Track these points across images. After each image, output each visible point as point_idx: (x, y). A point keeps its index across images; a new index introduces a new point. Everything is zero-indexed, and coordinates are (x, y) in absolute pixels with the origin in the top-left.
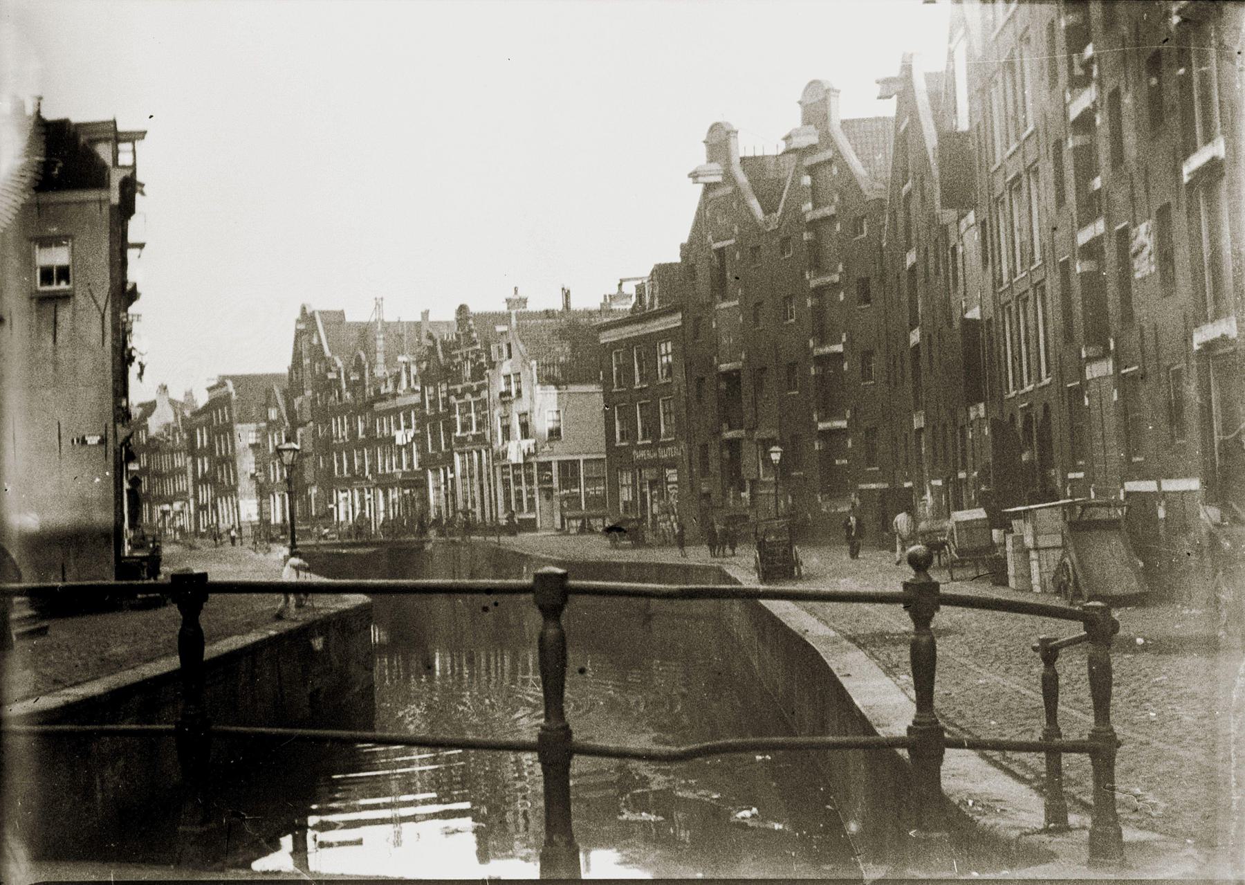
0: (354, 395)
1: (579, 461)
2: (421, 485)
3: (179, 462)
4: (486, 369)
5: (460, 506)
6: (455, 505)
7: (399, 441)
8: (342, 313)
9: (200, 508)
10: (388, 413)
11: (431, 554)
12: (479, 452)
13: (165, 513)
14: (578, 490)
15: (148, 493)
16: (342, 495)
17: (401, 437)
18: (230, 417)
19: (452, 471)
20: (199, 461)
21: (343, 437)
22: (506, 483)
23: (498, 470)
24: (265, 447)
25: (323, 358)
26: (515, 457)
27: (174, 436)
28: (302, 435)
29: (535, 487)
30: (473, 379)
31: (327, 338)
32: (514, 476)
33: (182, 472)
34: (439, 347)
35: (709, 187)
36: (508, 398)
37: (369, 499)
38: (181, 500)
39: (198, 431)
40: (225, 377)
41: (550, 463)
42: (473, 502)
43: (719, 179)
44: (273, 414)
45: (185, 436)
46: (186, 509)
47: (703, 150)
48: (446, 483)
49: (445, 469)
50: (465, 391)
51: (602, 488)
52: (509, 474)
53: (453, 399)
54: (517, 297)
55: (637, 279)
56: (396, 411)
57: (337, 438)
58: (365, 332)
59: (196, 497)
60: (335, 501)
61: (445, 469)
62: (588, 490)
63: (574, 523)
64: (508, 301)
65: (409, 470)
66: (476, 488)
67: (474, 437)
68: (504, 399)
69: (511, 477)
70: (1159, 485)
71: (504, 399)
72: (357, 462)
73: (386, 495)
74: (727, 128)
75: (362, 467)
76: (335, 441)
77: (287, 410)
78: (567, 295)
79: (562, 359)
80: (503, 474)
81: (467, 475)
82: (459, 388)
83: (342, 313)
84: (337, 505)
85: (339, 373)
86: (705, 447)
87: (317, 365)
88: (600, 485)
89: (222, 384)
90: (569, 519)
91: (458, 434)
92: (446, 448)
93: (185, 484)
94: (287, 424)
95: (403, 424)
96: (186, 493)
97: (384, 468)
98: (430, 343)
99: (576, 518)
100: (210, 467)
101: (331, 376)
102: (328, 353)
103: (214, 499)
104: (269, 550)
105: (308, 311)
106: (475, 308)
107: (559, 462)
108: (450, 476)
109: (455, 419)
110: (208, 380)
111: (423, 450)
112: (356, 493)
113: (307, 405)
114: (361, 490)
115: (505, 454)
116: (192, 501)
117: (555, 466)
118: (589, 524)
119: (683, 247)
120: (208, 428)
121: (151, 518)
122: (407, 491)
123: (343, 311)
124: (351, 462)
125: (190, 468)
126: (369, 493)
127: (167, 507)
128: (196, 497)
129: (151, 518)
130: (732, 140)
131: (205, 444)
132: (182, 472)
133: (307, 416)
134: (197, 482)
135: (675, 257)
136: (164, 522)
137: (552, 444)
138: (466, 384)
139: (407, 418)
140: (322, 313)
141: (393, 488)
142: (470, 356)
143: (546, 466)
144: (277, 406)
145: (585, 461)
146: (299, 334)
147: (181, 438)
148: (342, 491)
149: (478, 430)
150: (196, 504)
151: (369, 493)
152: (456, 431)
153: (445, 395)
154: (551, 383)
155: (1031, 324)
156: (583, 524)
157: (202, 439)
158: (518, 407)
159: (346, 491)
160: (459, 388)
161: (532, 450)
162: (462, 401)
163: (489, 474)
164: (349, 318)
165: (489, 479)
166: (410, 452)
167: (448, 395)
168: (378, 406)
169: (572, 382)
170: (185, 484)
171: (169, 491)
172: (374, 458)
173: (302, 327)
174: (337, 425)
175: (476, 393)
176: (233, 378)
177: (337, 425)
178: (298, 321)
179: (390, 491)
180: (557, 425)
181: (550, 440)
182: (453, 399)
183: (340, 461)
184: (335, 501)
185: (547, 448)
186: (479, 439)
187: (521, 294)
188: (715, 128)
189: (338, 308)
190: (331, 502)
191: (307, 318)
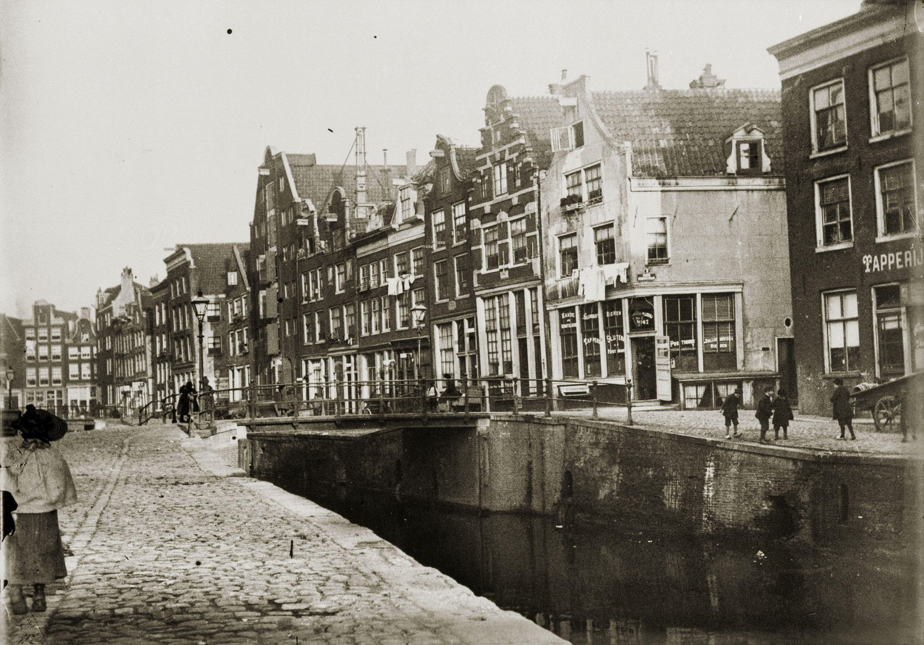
0: (330, 244)
1: (694, 296)
3: (139, 342)
4: (534, 170)
5: (485, 371)
6: (474, 372)
7: (392, 291)
8: (313, 157)
9: (159, 387)
10: (373, 258)
11: (486, 438)
12: (520, 294)
13: (126, 394)
14: (692, 342)
15: (112, 376)
16: (312, 367)
17: (394, 286)
19: (473, 322)
20: (158, 339)
21: (316, 296)
22: (568, 337)
23: (554, 317)
24: (225, 320)
25: (293, 205)
26: (593, 292)
27: (134, 315)
28: (264, 297)
29: (626, 339)
30: (511, 189)
31: (296, 182)
32: (582, 321)
33: (142, 351)
34: (453, 157)
36: (576, 206)
37: (349, 369)
38: (140, 380)
39: (157, 308)
41: (651, 298)
42: (508, 366)
44: (232, 279)
45: (144, 314)
46: (144, 390)
48: (461, 342)
49: (460, 323)
50: (496, 209)
51: (730, 338)
52: (574, 320)
56: (387, 254)
57: (308, 298)
58: (339, 176)
59: (154, 377)
60: (304, 374)
61: (460, 323)
62: (708, 341)
63: (691, 391)
66: (515, 345)
67: (511, 271)
68: (568, 208)
69: (577, 325)
70: (595, 413)
71: (568, 208)
72: (333, 325)
73: (371, 363)
75: (340, 330)
76: (305, 302)
77: (248, 273)
78: (652, 58)
79: (663, 144)
80: (562, 321)
81: (497, 329)
82: (487, 207)
83: (313, 157)
84: (307, 378)
85: (310, 219)
87: (283, 215)
88: (726, 335)
89: (180, 251)
90: (686, 384)
91: (484, 271)
92: (463, 291)
93: (144, 364)
94: (248, 289)
95: (397, 269)
96: (145, 373)
97: (369, 329)
99: (696, 384)
100: (168, 345)
101: (300, 222)
103: (171, 378)
104: (214, 432)
105: (274, 153)
107: (664, 297)
108: (468, 330)
109: (480, 250)
110: (166, 249)
111: (428, 300)
112: (332, 363)
113: (271, 266)
114: (338, 358)
115: (572, 291)
116: (150, 381)
117: (658, 305)
118: (717, 393)
120: (166, 303)
121: (114, 401)
122: (404, 355)
123: (314, 155)
124: (325, 325)
125: (149, 347)
126: (349, 361)
127: (127, 388)
128: (154, 377)
129: (114, 401)
131: (164, 320)
132: (142, 351)
133: (270, 276)
134: (156, 361)
136: (125, 402)
137: (654, 269)
139: (404, 264)
140: (288, 156)
141: (382, 353)
142: (507, 157)
143: (642, 305)
144: (237, 269)
145: (703, 295)
147: (140, 316)
148: (313, 361)
149: (517, 261)
150: (154, 384)
151: (349, 361)
152: (480, 268)
153: (462, 221)
154: (651, 175)
156: (708, 392)
157: (160, 317)
158: (593, 216)
159: (318, 361)
160: (487, 207)
161: (624, 279)
163: (535, 325)
164: (320, 161)
165: (535, 330)
166: (407, 305)
168: (361, 251)
169: (685, 175)
170: (144, 364)
171: (129, 373)
172: (357, 315)
173: (266, 172)
174: (307, 283)
176: (189, 247)
177: (307, 283)
179: (378, 357)
180: (661, 240)
181: (651, 264)
183: (311, 326)
184: (304, 374)
185: (647, 276)
189: (308, 152)
190: (299, 375)
191: (272, 161)
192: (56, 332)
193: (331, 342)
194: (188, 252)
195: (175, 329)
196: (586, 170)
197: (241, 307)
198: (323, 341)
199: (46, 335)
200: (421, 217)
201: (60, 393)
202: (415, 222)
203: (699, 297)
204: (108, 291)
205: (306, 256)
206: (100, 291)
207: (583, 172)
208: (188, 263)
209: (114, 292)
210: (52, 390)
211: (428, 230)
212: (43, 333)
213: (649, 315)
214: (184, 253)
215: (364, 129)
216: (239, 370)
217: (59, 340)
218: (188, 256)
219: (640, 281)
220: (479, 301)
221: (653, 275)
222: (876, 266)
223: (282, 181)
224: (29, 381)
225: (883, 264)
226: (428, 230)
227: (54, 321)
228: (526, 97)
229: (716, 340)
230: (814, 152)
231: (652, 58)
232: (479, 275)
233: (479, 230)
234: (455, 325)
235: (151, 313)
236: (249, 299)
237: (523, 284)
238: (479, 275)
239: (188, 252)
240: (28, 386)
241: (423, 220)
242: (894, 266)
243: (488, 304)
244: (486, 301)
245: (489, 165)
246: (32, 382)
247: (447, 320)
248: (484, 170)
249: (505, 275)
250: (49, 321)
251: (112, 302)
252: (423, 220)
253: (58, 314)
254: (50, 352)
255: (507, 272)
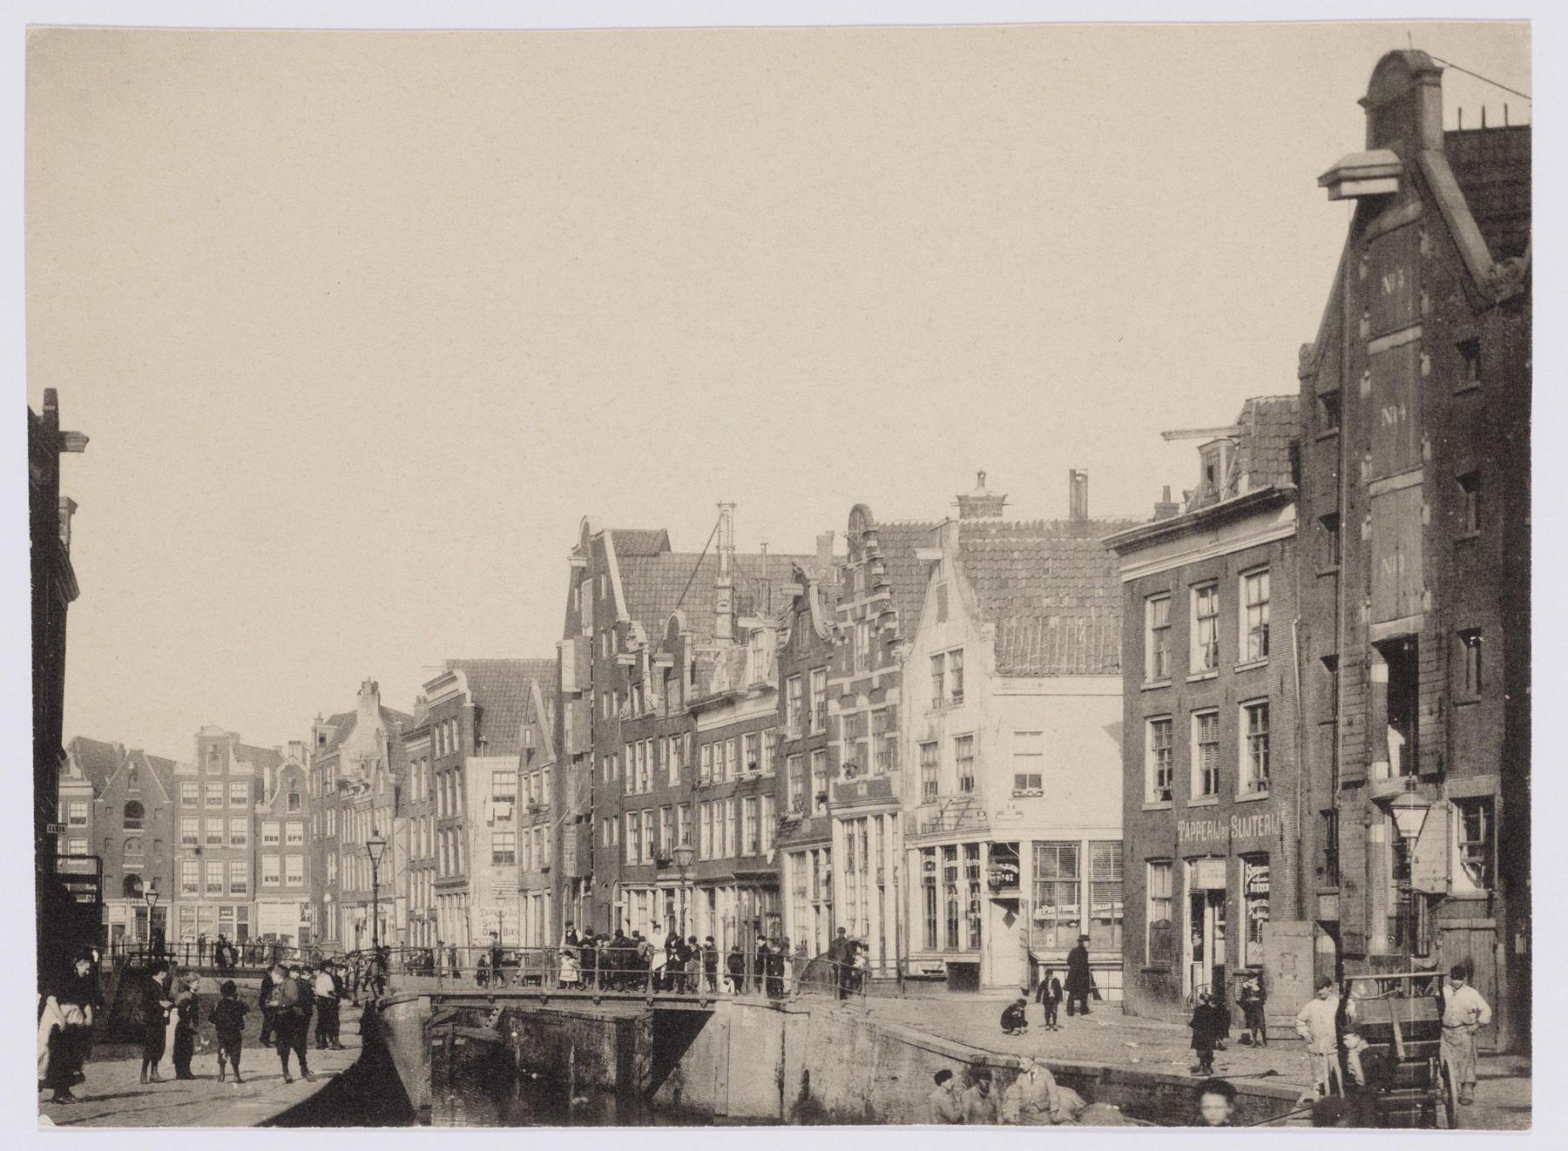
2: (770, 885)
18: (461, 743)
35: (1370, 207)
40: (453, 664)
43: (1390, 185)
47: (1359, 120)
53: (834, 706)
54: (983, 494)
55: (1201, 432)
64: (962, 501)
65: (754, 854)
67: (872, 786)
72: (665, 834)
74: (1414, 64)
78: (1078, 480)
82: (846, 683)
85: (639, 653)
86: (1331, 814)
98: (798, 589)
102: (623, 615)
106: (882, 515)
119: (1305, 354)
130: (1427, 92)
135: (1285, 383)
138: (860, 675)
140: (618, 536)
146: (580, 575)
147: (385, 779)
155: (717, 828)
157: (417, 788)
160: (846, 683)
162: (851, 711)
167: (827, 699)
175: (876, 694)
178: (577, 552)
182: (834, 706)
186: (880, 790)
187: (994, 487)
188: (1392, 63)
191: (592, 546)
192: (242, 790)
193: (662, 864)
194: (460, 674)
195: (605, 655)
196: (951, 653)
197: (540, 787)
198: (1213, 800)
199: (277, 833)
200: (775, 684)
201: (243, 912)
202: (766, 691)
203: (842, 721)
204: (332, 721)
205: (633, 716)
206: (319, 719)
207: (947, 656)
208: (462, 697)
209: (345, 724)
210: (227, 904)
211: (782, 706)
212: (216, 790)
213: (1013, 868)
214: (454, 679)
215: (733, 505)
216: (535, 897)
217: (244, 806)
218: (462, 685)
219: (1000, 821)
220: (836, 824)
221: (1019, 813)
222: (1187, 835)
223: (603, 578)
224: (185, 886)
225: (1193, 833)
226: (782, 706)
227: (236, 768)
228: (905, 523)
229: (1109, 906)
230: (1147, 681)
231: (1078, 480)
232: (835, 784)
233: (837, 716)
234: (809, 856)
235: (403, 776)
236: (552, 775)
237: (882, 807)
238: (835, 784)
239: (460, 674)
240: (185, 894)
241: (777, 687)
242: (1200, 836)
243: (846, 829)
244: (845, 824)
245: (850, 623)
246: (193, 889)
247: (799, 848)
248: (845, 628)
249: (862, 791)
250: (226, 767)
251: (340, 746)
252: (777, 687)
253: (243, 752)
254: (226, 829)
255: (865, 786)
